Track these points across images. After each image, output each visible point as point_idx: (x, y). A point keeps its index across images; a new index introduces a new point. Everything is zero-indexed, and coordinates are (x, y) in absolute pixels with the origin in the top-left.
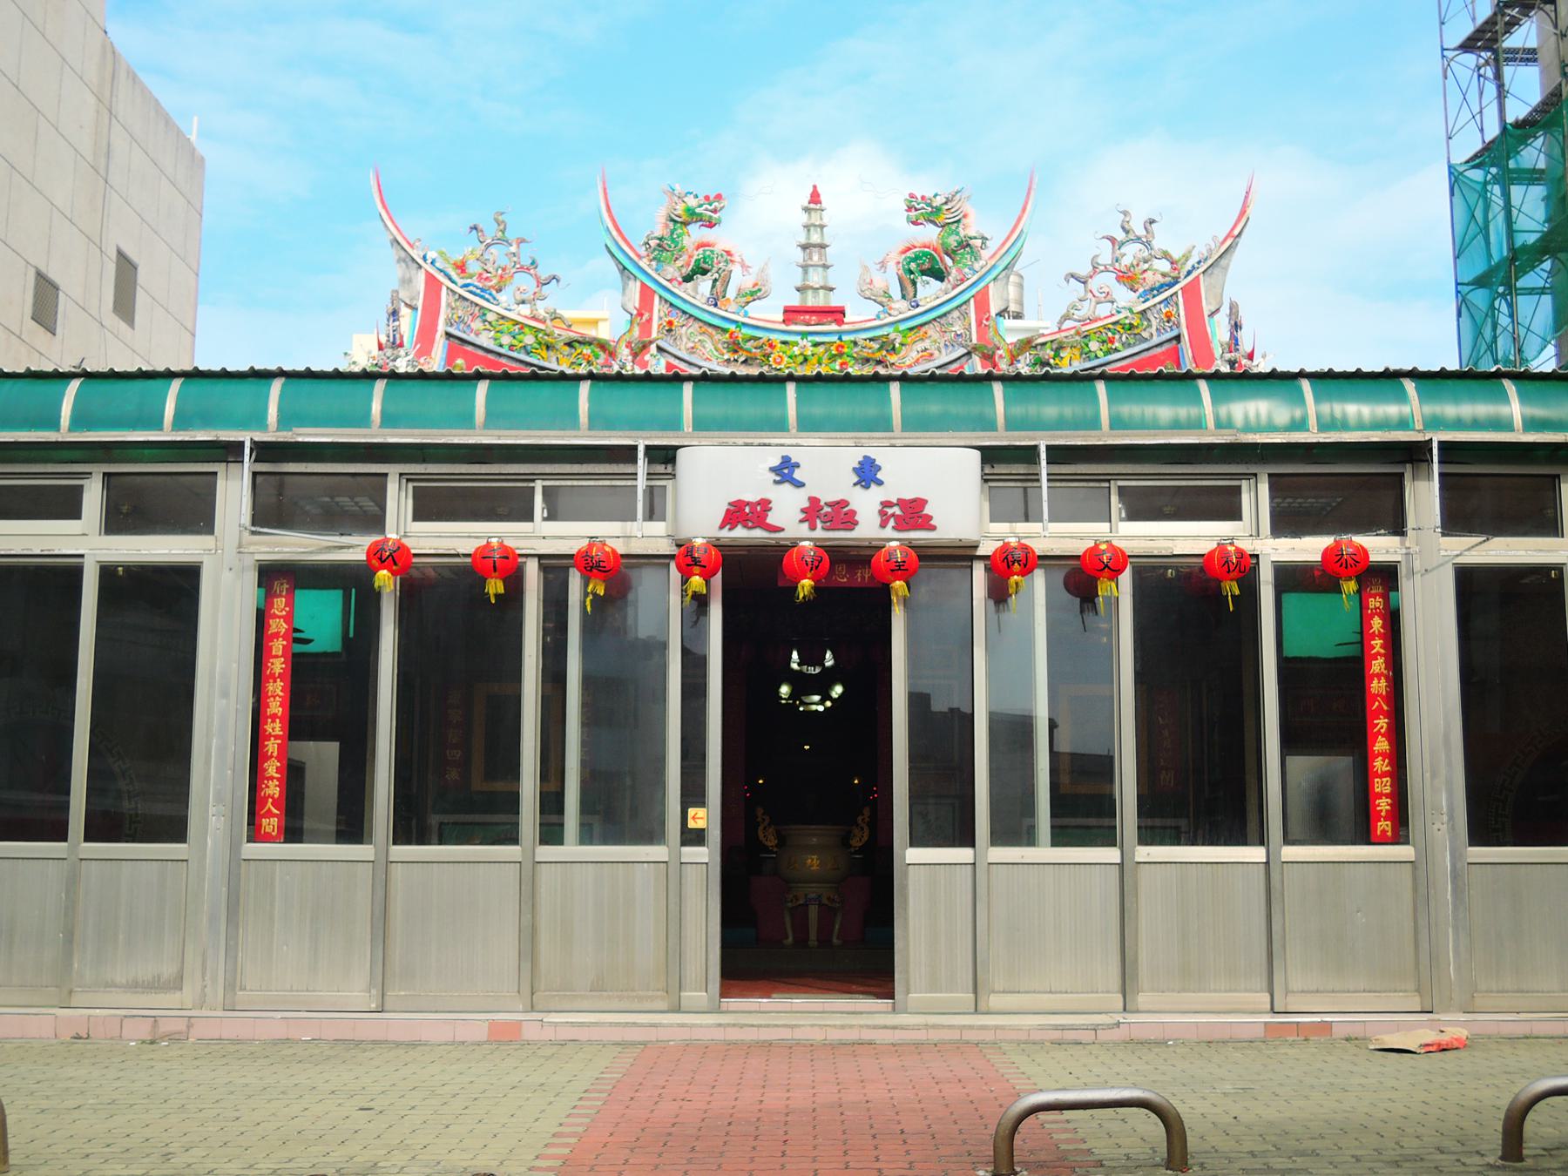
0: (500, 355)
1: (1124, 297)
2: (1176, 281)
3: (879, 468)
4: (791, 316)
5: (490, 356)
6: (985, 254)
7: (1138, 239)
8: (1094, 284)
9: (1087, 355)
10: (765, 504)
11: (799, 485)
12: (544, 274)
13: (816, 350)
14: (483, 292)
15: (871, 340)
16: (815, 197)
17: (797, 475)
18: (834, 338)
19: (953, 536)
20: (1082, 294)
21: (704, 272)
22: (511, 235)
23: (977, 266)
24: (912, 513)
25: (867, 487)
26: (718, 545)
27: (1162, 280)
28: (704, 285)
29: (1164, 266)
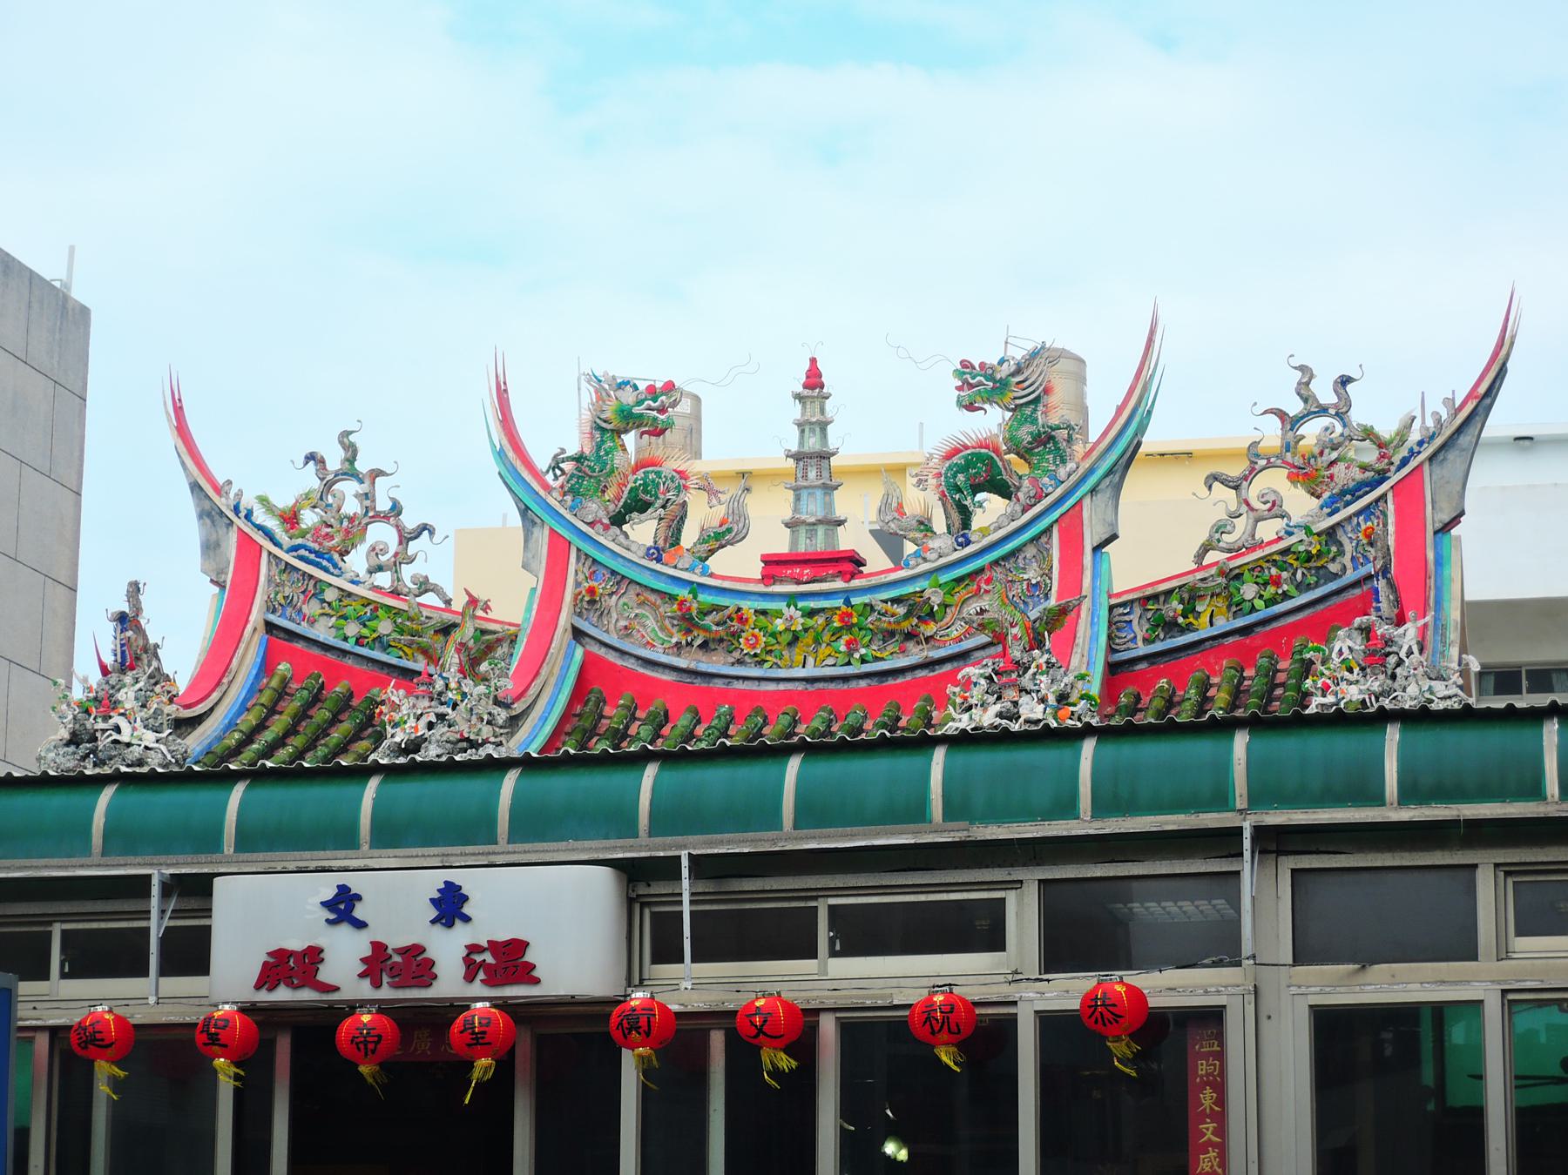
0: (344, 653)
1: (1301, 504)
2: (1382, 477)
3: (465, 898)
4: (774, 570)
5: (330, 656)
6: (1079, 449)
7: (1323, 410)
8: (1254, 491)
9: (1237, 607)
10: (314, 955)
11: (360, 925)
12: (410, 521)
13: (810, 622)
14: (320, 557)
15: (895, 601)
16: (814, 379)
17: (359, 912)
18: (839, 602)
19: (562, 993)
20: (1233, 508)
21: (643, 507)
22: (362, 465)
23: (1062, 473)
24: (508, 960)
25: (450, 925)
26: (248, 1009)
27: (1359, 476)
28: (643, 531)
29: (1370, 455)
